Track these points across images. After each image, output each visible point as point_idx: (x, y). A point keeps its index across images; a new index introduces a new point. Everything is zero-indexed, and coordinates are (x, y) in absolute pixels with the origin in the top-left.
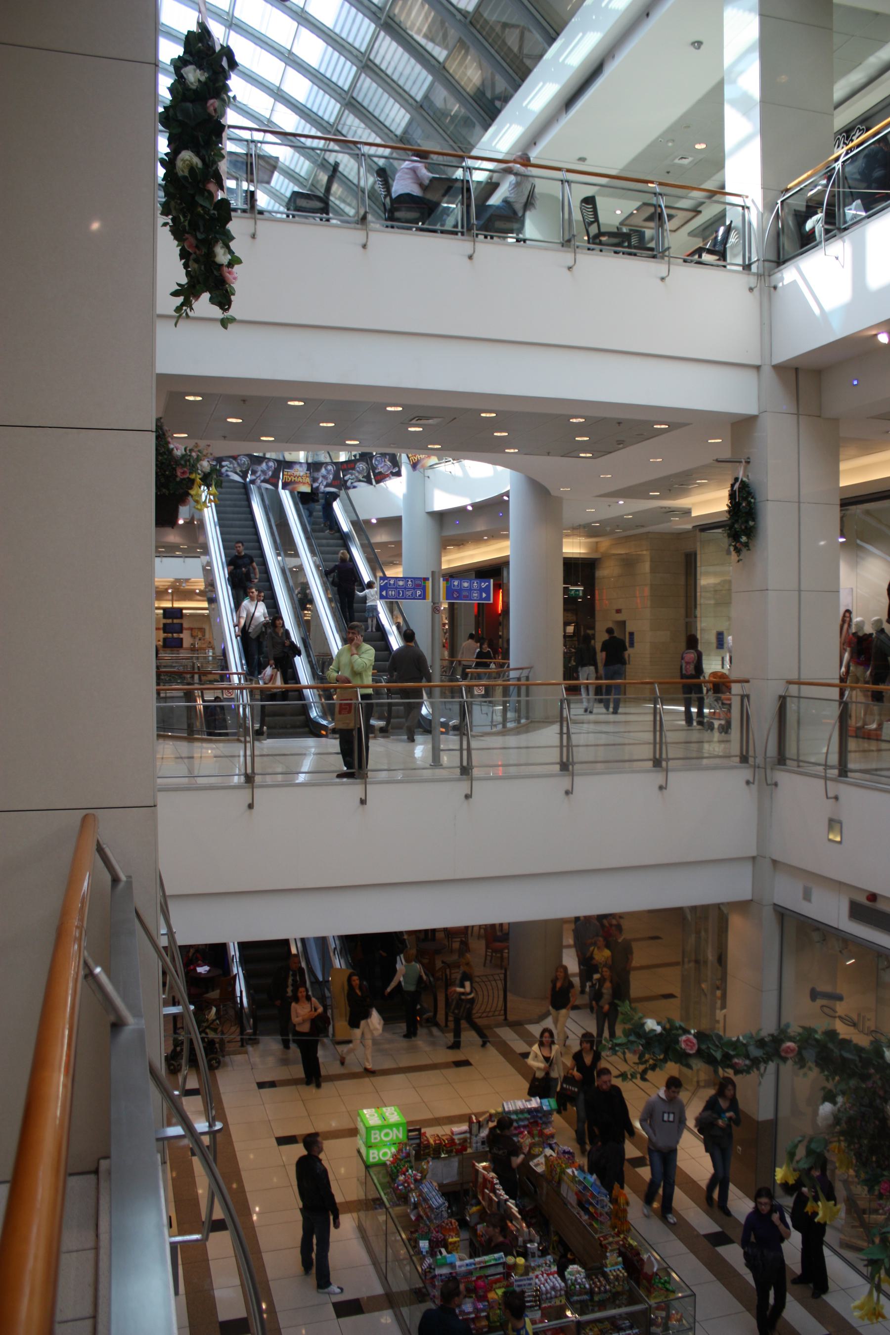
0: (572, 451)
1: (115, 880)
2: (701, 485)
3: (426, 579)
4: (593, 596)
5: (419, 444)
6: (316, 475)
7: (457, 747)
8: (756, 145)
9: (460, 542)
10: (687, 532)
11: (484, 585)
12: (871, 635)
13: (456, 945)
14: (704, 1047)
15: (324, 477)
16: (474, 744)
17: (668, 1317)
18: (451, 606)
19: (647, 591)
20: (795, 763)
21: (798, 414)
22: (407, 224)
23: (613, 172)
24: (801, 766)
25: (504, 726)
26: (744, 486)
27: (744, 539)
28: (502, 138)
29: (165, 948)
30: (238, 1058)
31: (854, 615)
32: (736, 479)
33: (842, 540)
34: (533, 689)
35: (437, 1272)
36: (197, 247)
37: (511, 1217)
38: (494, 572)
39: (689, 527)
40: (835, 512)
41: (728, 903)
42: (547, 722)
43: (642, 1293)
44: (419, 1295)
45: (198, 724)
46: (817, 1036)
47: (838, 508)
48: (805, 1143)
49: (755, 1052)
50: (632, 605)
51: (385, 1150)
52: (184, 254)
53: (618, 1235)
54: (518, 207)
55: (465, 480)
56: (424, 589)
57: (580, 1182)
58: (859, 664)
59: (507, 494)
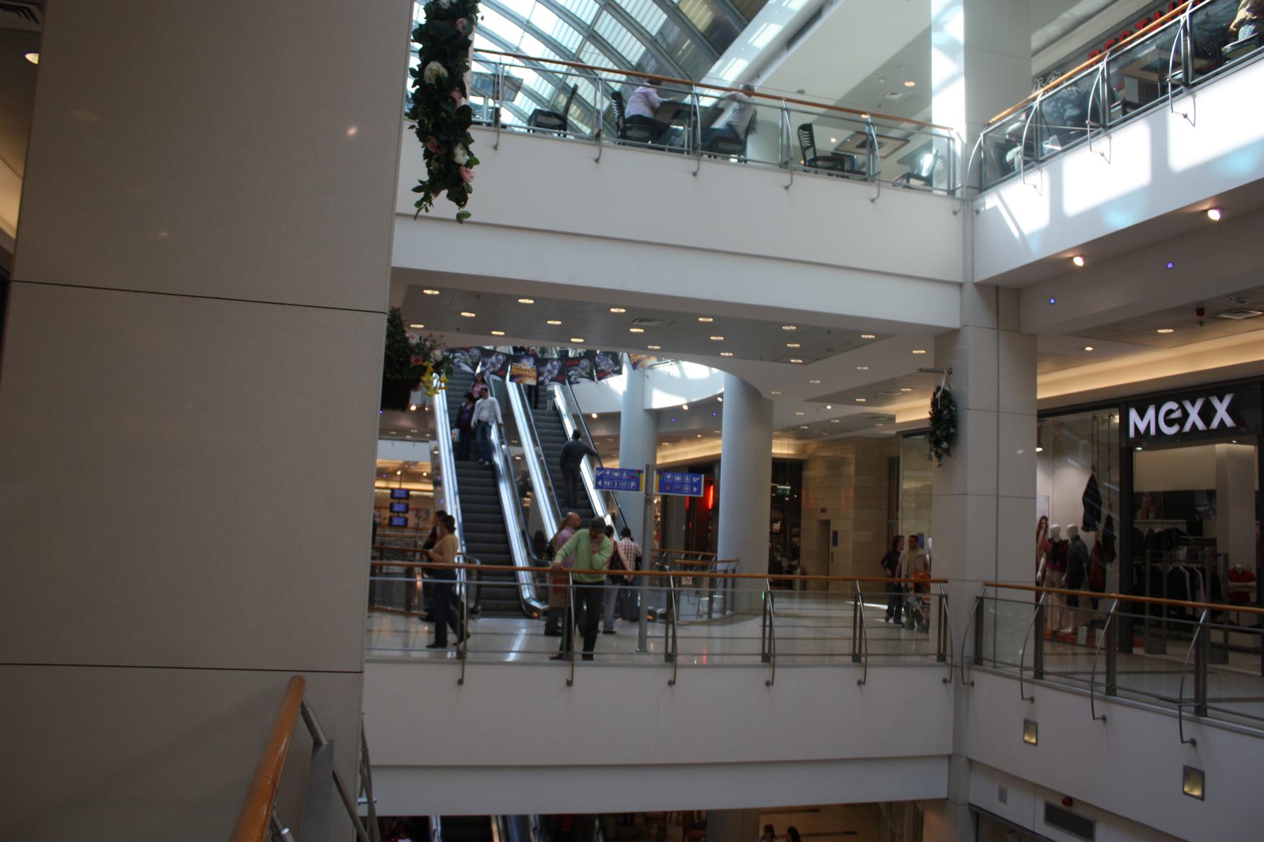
0: (783, 356)
1: (317, 743)
2: (905, 393)
3: (640, 472)
4: (800, 495)
5: (638, 344)
6: (541, 369)
7: (663, 634)
8: (960, 87)
9: (675, 439)
10: (891, 438)
11: (695, 480)
12: (1066, 541)
13: (654, 831)
15: (550, 372)
16: (679, 632)
18: (664, 498)
19: (851, 493)
20: (991, 664)
21: (998, 329)
22: (640, 143)
23: (831, 103)
24: (997, 668)
25: (710, 616)
26: (946, 395)
27: (945, 445)
28: (730, 70)
29: (364, 819)
31: (1050, 522)
32: (939, 389)
33: (1039, 450)
34: (739, 581)
36: (438, 147)
38: (707, 468)
39: (893, 432)
40: (1033, 422)
41: (924, 801)
42: (751, 614)
45: (416, 601)
47: (1035, 418)
50: (836, 503)
52: (427, 155)
54: (741, 131)
55: (683, 380)
56: (638, 481)
58: (1054, 568)
59: (721, 395)
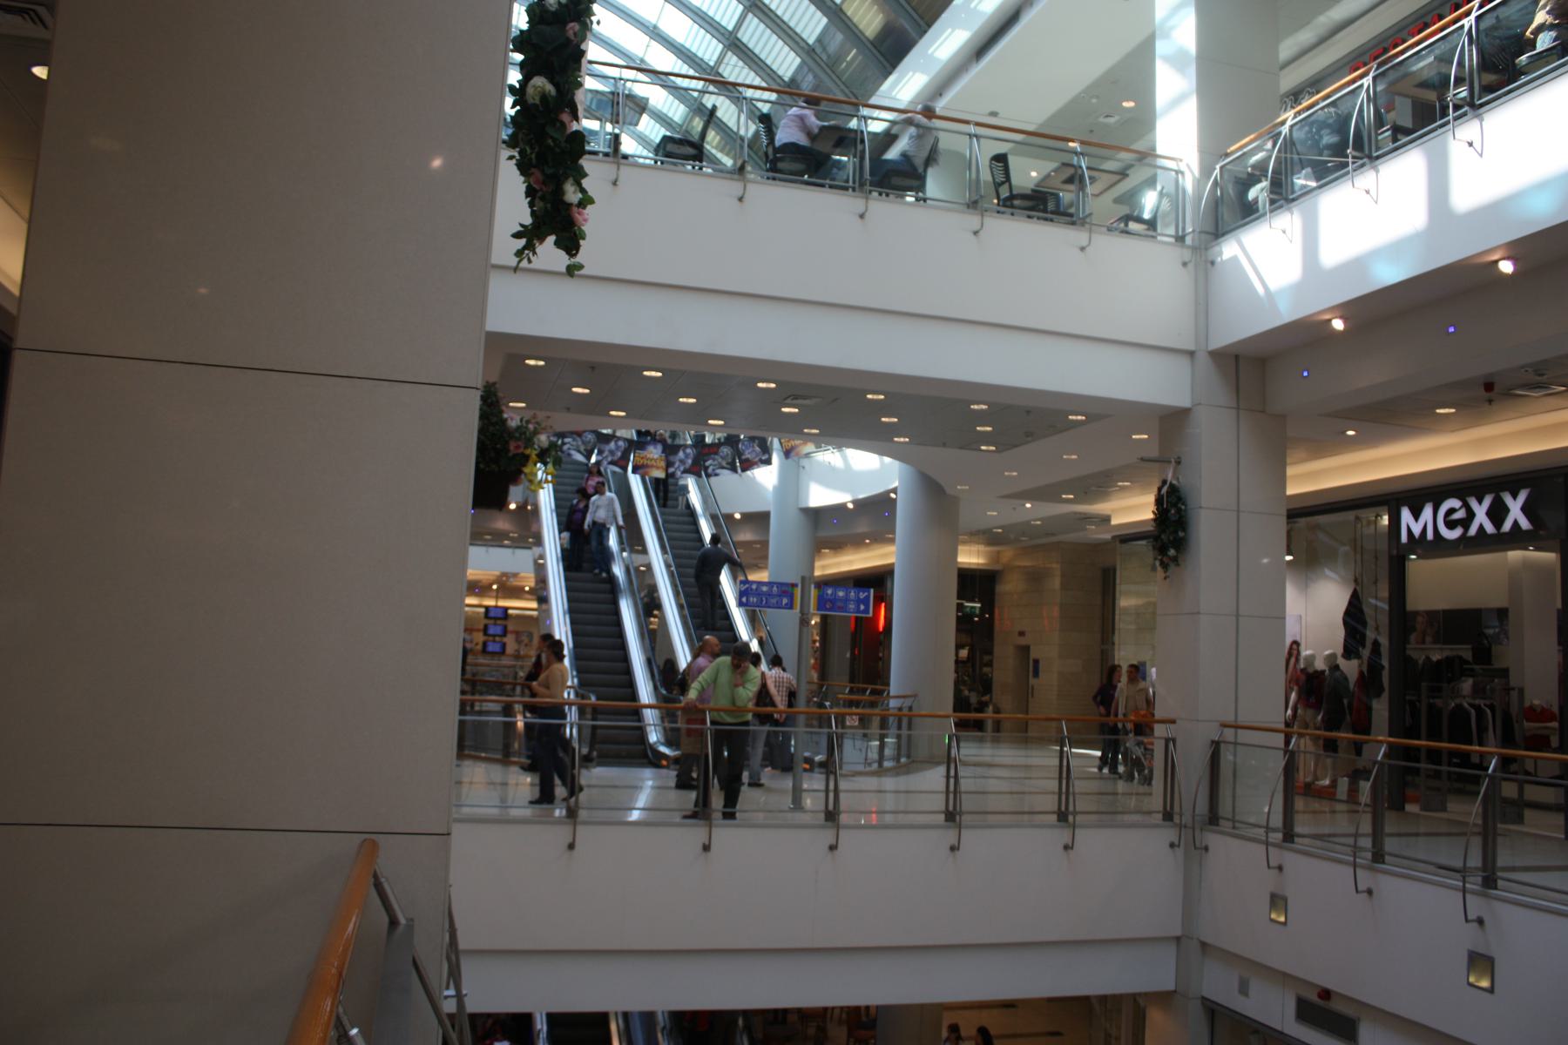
0: (972, 442)
1: (393, 922)
2: (1123, 488)
3: (794, 585)
4: (992, 614)
5: (792, 428)
6: (671, 458)
7: (822, 787)
8: (1191, 108)
9: (837, 545)
10: (1105, 543)
11: (862, 595)
12: (1323, 672)
13: (811, 1031)
15: (682, 461)
16: (843, 785)
18: (824, 618)
19: (1056, 611)
20: (1230, 824)
21: (1238, 408)
22: (793, 177)
23: (1031, 128)
24: (1237, 828)
25: (880, 765)
26: (1174, 490)
27: (1172, 552)
28: (905, 86)
29: (451, 1016)
31: (1302, 647)
32: (1164, 482)
33: (1289, 558)
34: (916, 721)
36: (544, 183)
38: (877, 581)
39: (1108, 536)
40: (1281, 524)
41: (1146, 994)
42: (932, 762)
45: (516, 745)
47: (1284, 519)
50: (1037, 624)
52: (530, 192)
54: (919, 162)
55: (848, 472)
56: (791, 597)
58: (1308, 705)
59: (894, 491)
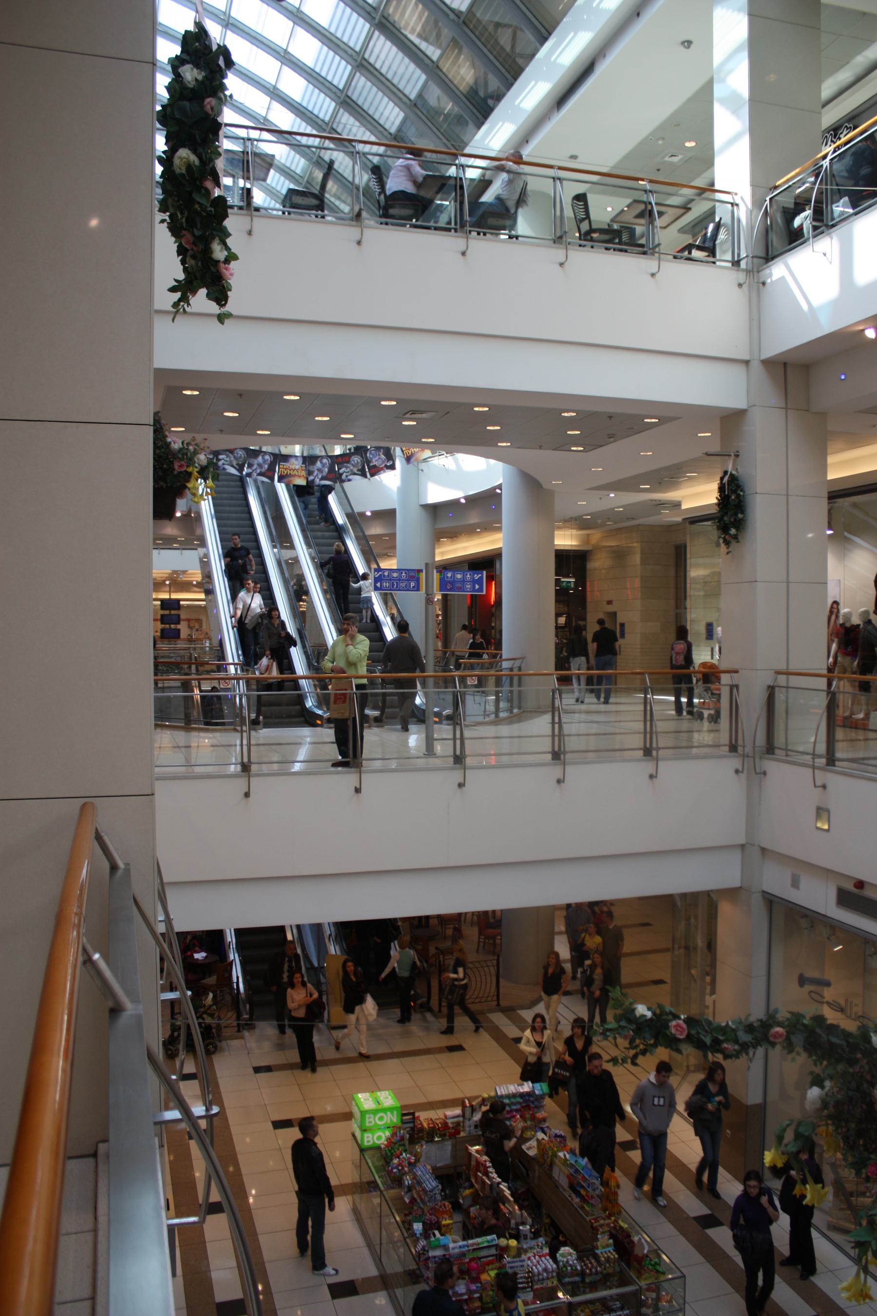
0: (563, 444)
1: (114, 868)
2: (690, 478)
3: (420, 571)
4: (584, 588)
5: (413, 438)
6: (311, 468)
7: (451, 736)
8: (745, 143)
9: (453, 534)
10: (677, 524)
11: (477, 577)
12: (858, 626)
13: (449, 932)
14: (693, 1032)
15: (319, 470)
16: (467, 733)
17: (658, 1299)
18: (445, 597)
19: (637, 583)
20: (784, 752)
21: (786, 408)
22: (401, 221)
23: (604, 170)
24: (789, 756)
25: (497, 716)
26: (733, 479)
27: (733, 531)
28: (495, 136)
29: (163, 935)
30: (235, 1043)
31: (841, 606)
32: (726, 473)
33: (830, 532)
34: (525, 679)
35: (431, 1254)
36: (194, 243)
37: (504, 1200)
38: (487, 563)
39: (679, 519)
40: (823, 505)
41: (718, 890)
42: (539, 711)
43: (633, 1274)
44: (413, 1277)
45: (195, 713)
46: (805, 1021)
47: (826, 501)
48: (793, 1126)
49: (744, 1037)
50: (623, 596)
51: (380, 1133)
52: (181, 251)
53: (609, 1217)
54: (511, 204)
55: (459, 473)
56: (418, 581)
57: (572, 1166)
58: (846, 654)
59: (500, 487)
